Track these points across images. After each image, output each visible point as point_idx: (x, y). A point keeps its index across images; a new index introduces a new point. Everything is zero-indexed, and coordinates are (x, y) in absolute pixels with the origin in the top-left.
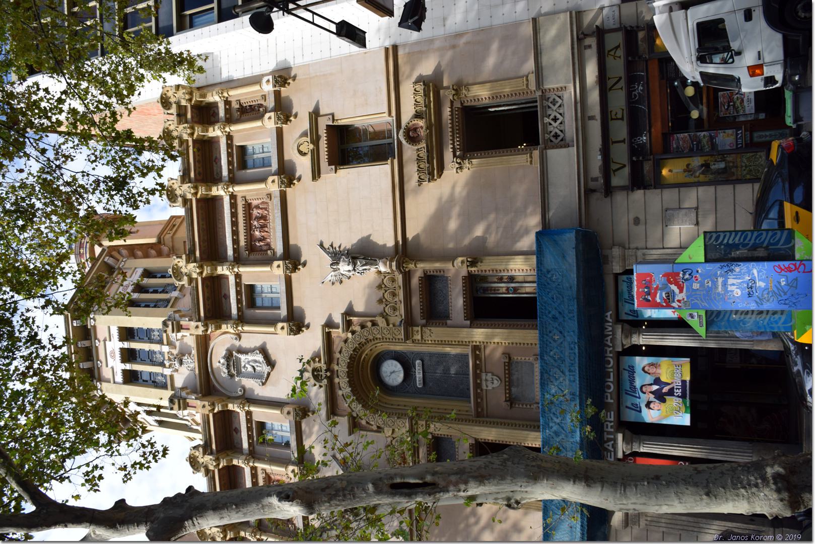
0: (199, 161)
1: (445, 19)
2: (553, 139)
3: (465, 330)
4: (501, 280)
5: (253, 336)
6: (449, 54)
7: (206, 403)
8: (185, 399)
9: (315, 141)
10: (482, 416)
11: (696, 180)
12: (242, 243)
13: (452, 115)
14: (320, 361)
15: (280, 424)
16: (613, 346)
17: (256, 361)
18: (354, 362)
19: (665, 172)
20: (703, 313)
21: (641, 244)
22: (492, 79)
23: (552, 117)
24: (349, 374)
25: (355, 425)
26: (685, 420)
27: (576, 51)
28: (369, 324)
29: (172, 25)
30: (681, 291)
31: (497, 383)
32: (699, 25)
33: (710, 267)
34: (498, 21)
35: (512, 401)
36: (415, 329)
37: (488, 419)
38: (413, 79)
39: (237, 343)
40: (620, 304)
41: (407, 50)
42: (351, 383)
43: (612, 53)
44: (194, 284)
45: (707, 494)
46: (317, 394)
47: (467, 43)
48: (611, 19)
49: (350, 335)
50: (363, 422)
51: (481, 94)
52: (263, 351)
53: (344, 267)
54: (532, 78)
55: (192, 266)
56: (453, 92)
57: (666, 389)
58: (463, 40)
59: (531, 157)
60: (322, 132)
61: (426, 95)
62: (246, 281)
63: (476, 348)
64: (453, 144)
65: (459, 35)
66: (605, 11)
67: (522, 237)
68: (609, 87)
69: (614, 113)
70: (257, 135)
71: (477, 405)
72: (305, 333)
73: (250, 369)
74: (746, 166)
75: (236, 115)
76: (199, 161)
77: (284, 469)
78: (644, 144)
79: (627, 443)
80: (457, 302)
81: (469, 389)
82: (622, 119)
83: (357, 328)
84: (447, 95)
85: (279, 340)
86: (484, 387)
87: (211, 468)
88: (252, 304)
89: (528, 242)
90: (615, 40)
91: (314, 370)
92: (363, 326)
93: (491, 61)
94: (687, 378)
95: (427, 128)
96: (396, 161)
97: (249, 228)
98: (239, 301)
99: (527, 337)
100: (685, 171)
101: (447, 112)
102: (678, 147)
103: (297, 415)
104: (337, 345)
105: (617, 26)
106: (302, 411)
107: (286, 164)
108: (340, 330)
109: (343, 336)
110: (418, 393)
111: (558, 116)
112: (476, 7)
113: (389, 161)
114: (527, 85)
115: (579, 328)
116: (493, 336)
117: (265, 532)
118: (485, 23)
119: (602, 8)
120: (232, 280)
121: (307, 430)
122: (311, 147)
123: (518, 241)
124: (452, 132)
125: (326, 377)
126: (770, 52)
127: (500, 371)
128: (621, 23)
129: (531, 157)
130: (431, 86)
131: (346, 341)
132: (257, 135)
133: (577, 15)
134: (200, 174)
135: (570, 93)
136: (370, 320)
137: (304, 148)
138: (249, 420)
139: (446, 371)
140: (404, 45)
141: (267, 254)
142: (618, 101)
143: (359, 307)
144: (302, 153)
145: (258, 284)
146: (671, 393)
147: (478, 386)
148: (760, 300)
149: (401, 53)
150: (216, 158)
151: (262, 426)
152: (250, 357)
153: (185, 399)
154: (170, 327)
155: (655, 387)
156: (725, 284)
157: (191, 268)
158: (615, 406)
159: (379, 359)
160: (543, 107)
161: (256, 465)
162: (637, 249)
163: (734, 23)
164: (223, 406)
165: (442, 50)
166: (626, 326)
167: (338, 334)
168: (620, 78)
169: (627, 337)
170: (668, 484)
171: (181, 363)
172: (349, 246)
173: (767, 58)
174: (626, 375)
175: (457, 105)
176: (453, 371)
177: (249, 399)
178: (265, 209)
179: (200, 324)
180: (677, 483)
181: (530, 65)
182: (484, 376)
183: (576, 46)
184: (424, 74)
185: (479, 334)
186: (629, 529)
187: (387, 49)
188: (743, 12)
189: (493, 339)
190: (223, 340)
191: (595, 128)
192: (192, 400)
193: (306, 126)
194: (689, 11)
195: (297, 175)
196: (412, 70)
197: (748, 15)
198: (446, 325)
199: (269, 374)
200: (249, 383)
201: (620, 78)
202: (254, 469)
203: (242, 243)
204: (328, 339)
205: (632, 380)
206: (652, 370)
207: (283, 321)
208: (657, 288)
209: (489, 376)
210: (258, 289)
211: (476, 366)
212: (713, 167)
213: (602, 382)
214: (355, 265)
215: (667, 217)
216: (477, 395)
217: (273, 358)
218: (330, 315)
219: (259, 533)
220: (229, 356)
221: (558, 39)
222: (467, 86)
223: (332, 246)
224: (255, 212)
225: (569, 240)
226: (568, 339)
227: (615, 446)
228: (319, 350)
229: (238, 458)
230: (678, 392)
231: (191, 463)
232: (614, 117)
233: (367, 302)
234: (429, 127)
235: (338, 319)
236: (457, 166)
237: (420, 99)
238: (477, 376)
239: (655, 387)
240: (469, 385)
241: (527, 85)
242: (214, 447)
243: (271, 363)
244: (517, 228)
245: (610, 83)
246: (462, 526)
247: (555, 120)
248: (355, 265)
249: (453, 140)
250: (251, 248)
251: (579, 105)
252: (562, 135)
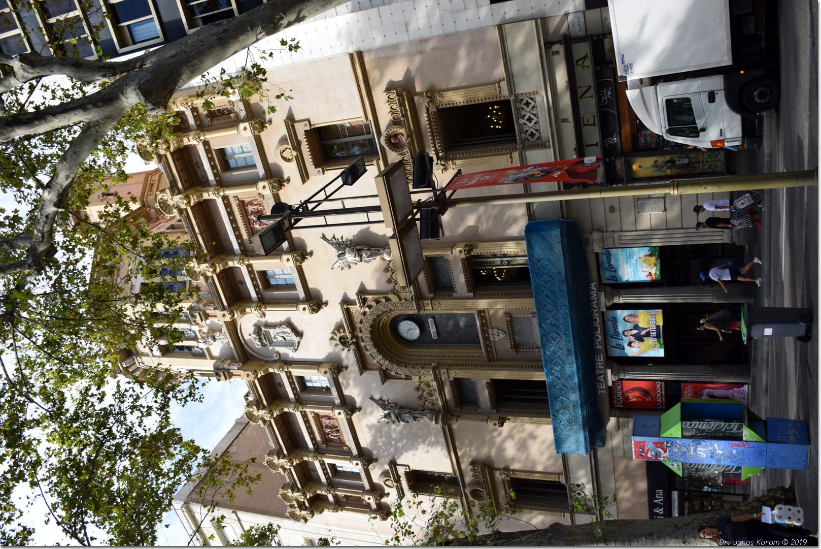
0: (182, 171)
1: (407, 25)
2: (529, 138)
3: (471, 301)
4: (495, 256)
5: (275, 315)
6: (418, 59)
7: (250, 373)
8: (228, 370)
9: (297, 147)
10: (493, 359)
11: (663, 174)
12: (318, 438)
13: (429, 120)
14: (344, 331)
15: (318, 379)
16: (599, 308)
17: (285, 333)
18: (376, 331)
19: (635, 167)
20: (680, 464)
21: (617, 228)
22: (464, 84)
23: (526, 117)
24: (372, 339)
25: (386, 376)
26: (660, 353)
27: (545, 59)
28: (383, 300)
29: (112, 39)
30: (665, 452)
31: (502, 336)
32: (667, 101)
33: (684, 440)
34: (463, 27)
35: (516, 346)
36: (426, 302)
37: (499, 363)
38: (384, 87)
39: (263, 320)
40: (601, 272)
41: (373, 56)
42: (376, 345)
43: (580, 63)
44: (210, 281)
45: (684, 543)
46: (348, 357)
47: (434, 49)
48: (576, 25)
49: (367, 309)
50: (393, 373)
51: (457, 98)
52: (289, 324)
53: (350, 257)
54: (504, 85)
55: (177, 198)
56: (428, 100)
57: (643, 333)
58: (430, 46)
59: (511, 158)
60: (301, 137)
61: (402, 105)
62: (215, 146)
63: (480, 312)
64: (435, 146)
65: (424, 41)
66: (570, 18)
67: (511, 225)
68: (579, 95)
69: (585, 120)
70: (237, 141)
71: (488, 353)
72: (324, 310)
73: (280, 339)
74: (707, 162)
75: (207, 121)
76: (182, 171)
77: (254, 189)
78: (615, 145)
79: (615, 375)
80: (460, 279)
81: (478, 337)
82: (594, 125)
83: (374, 304)
84: (422, 103)
85: (300, 316)
86: (492, 339)
87: (209, 274)
88: (226, 166)
89: (518, 228)
90: (582, 50)
91: (340, 338)
92: (377, 302)
93: (461, 66)
94: (661, 324)
95: (408, 137)
96: (381, 162)
97: (248, 223)
98: (213, 167)
99: (523, 305)
100: (653, 167)
101: (424, 118)
102: (645, 143)
103: (333, 373)
104: (357, 318)
105: (582, 33)
106: (336, 368)
107: (347, 399)
108: (358, 306)
109: (362, 310)
110: (433, 343)
111: (532, 117)
112: (438, 12)
113: (375, 162)
114: (500, 92)
115: (569, 302)
116: (495, 304)
117: (252, 256)
118: (450, 29)
119: (567, 15)
120: (244, 270)
121: (345, 382)
122: (295, 153)
123: (508, 228)
124: (432, 136)
125: (353, 343)
126: (731, 131)
127: (504, 326)
128: (586, 30)
129: (511, 158)
130: (403, 91)
131: (364, 314)
132: (237, 141)
133: (542, 21)
134: (186, 182)
135: (542, 99)
136: (381, 295)
137: (287, 154)
138: (251, 272)
139: (457, 324)
140: (370, 51)
141: (230, 117)
142: (589, 107)
143: (371, 286)
144: (288, 160)
145: (228, 148)
146: (648, 335)
147: (486, 339)
148: (719, 460)
149: (367, 59)
150: (197, 163)
151: (263, 274)
152: (278, 330)
153: (228, 370)
154: (198, 317)
155: (635, 332)
156: (695, 450)
157: (178, 200)
158: (603, 350)
159: (395, 323)
160: (517, 110)
161: (251, 262)
162: (614, 231)
163: (699, 103)
164: (198, 197)
165: (410, 56)
166: (609, 289)
167: (356, 309)
168: (590, 87)
169: (609, 300)
170: (659, 538)
171: (214, 339)
172: (350, 237)
173: (728, 135)
174: (610, 324)
175: (433, 109)
176: (462, 324)
177: (287, 363)
178: (260, 204)
179: (226, 312)
180: (664, 537)
181: (500, 71)
182: (490, 331)
183: (544, 55)
184: (395, 79)
185: (483, 304)
186: (620, 431)
187: (351, 55)
188: (707, 94)
189: (494, 306)
190: (248, 321)
191: (569, 129)
192: (234, 369)
193: (283, 131)
194: (658, 87)
195: (285, 177)
196: (382, 76)
197: (712, 97)
198: (451, 297)
199: (299, 343)
200: (282, 350)
201: (590, 87)
202: (225, 198)
203: (318, 438)
204: (348, 314)
205: (615, 327)
206: (631, 319)
207: (243, 121)
208: (648, 450)
209: (495, 331)
210: (229, 151)
211: (482, 325)
212: (677, 163)
213: (592, 343)
214: (361, 256)
215: (639, 204)
216: (487, 346)
217: (300, 328)
218: (345, 294)
219: (246, 259)
220: (258, 330)
221: (526, 46)
222: (441, 91)
223: (334, 237)
224: (250, 208)
225: (555, 235)
226: (561, 311)
227: (605, 378)
228: (341, 321)
229: (207, 191)
230: (655, 334)
231: (140, 154)
232: (586, 123)
233: (377, 283)
234: (409, 136)
235: (353, 296)
236: (442, 167)
237: (396, 106)
238: (484, 332)
239: (635, 332)
240: (477, 334)
241: (500, 92)
242: (265, 402)
243: (299, 334)
244: (506, 218)
245: (580, 92)
246: (487, 438)
247: (527, 104)
248: (361, 256)
249: (434, 143)
250: (326, 440)
251: (552, 111)
252: (538, 135)
